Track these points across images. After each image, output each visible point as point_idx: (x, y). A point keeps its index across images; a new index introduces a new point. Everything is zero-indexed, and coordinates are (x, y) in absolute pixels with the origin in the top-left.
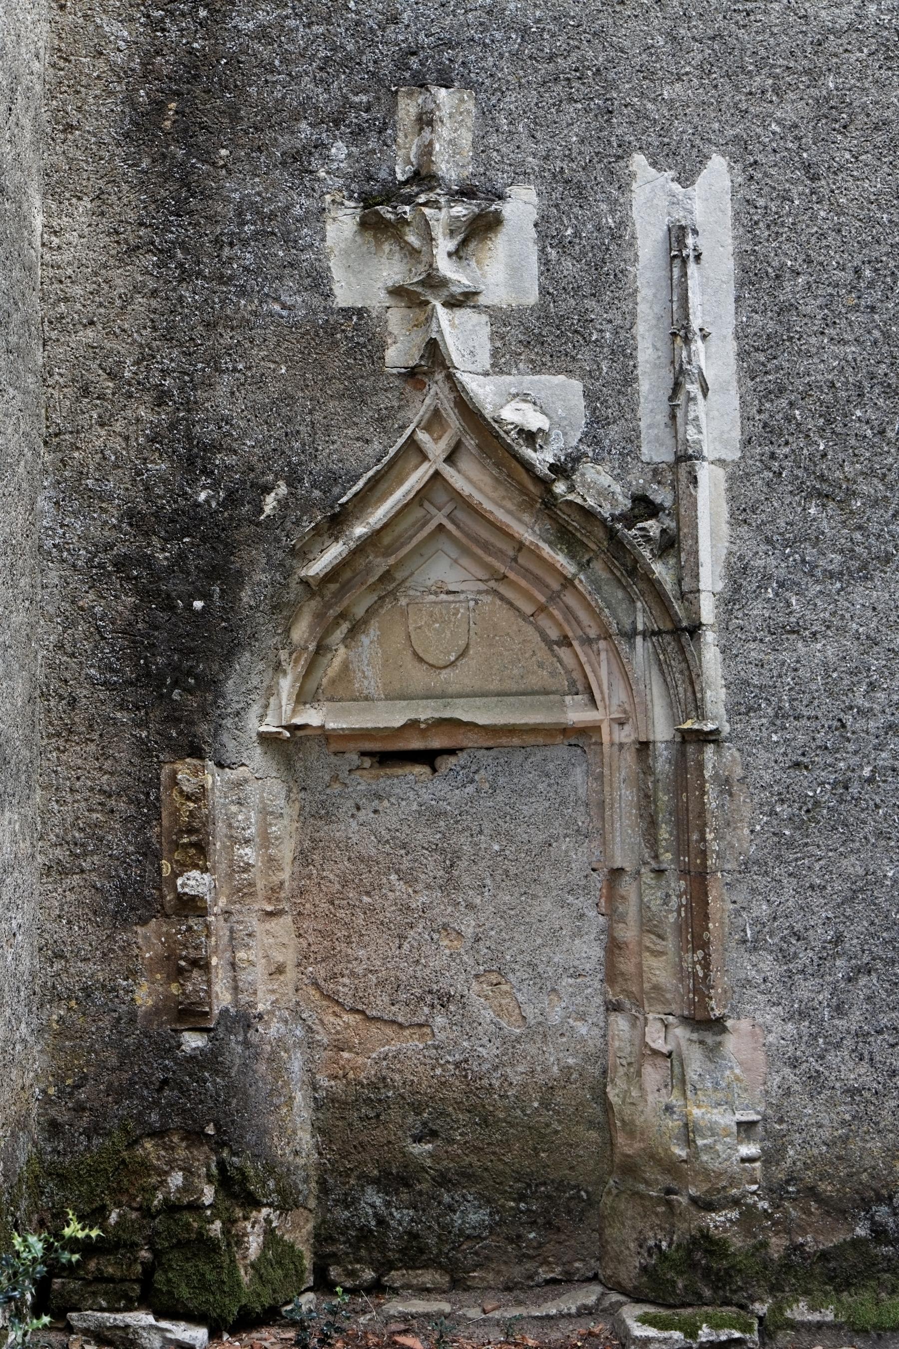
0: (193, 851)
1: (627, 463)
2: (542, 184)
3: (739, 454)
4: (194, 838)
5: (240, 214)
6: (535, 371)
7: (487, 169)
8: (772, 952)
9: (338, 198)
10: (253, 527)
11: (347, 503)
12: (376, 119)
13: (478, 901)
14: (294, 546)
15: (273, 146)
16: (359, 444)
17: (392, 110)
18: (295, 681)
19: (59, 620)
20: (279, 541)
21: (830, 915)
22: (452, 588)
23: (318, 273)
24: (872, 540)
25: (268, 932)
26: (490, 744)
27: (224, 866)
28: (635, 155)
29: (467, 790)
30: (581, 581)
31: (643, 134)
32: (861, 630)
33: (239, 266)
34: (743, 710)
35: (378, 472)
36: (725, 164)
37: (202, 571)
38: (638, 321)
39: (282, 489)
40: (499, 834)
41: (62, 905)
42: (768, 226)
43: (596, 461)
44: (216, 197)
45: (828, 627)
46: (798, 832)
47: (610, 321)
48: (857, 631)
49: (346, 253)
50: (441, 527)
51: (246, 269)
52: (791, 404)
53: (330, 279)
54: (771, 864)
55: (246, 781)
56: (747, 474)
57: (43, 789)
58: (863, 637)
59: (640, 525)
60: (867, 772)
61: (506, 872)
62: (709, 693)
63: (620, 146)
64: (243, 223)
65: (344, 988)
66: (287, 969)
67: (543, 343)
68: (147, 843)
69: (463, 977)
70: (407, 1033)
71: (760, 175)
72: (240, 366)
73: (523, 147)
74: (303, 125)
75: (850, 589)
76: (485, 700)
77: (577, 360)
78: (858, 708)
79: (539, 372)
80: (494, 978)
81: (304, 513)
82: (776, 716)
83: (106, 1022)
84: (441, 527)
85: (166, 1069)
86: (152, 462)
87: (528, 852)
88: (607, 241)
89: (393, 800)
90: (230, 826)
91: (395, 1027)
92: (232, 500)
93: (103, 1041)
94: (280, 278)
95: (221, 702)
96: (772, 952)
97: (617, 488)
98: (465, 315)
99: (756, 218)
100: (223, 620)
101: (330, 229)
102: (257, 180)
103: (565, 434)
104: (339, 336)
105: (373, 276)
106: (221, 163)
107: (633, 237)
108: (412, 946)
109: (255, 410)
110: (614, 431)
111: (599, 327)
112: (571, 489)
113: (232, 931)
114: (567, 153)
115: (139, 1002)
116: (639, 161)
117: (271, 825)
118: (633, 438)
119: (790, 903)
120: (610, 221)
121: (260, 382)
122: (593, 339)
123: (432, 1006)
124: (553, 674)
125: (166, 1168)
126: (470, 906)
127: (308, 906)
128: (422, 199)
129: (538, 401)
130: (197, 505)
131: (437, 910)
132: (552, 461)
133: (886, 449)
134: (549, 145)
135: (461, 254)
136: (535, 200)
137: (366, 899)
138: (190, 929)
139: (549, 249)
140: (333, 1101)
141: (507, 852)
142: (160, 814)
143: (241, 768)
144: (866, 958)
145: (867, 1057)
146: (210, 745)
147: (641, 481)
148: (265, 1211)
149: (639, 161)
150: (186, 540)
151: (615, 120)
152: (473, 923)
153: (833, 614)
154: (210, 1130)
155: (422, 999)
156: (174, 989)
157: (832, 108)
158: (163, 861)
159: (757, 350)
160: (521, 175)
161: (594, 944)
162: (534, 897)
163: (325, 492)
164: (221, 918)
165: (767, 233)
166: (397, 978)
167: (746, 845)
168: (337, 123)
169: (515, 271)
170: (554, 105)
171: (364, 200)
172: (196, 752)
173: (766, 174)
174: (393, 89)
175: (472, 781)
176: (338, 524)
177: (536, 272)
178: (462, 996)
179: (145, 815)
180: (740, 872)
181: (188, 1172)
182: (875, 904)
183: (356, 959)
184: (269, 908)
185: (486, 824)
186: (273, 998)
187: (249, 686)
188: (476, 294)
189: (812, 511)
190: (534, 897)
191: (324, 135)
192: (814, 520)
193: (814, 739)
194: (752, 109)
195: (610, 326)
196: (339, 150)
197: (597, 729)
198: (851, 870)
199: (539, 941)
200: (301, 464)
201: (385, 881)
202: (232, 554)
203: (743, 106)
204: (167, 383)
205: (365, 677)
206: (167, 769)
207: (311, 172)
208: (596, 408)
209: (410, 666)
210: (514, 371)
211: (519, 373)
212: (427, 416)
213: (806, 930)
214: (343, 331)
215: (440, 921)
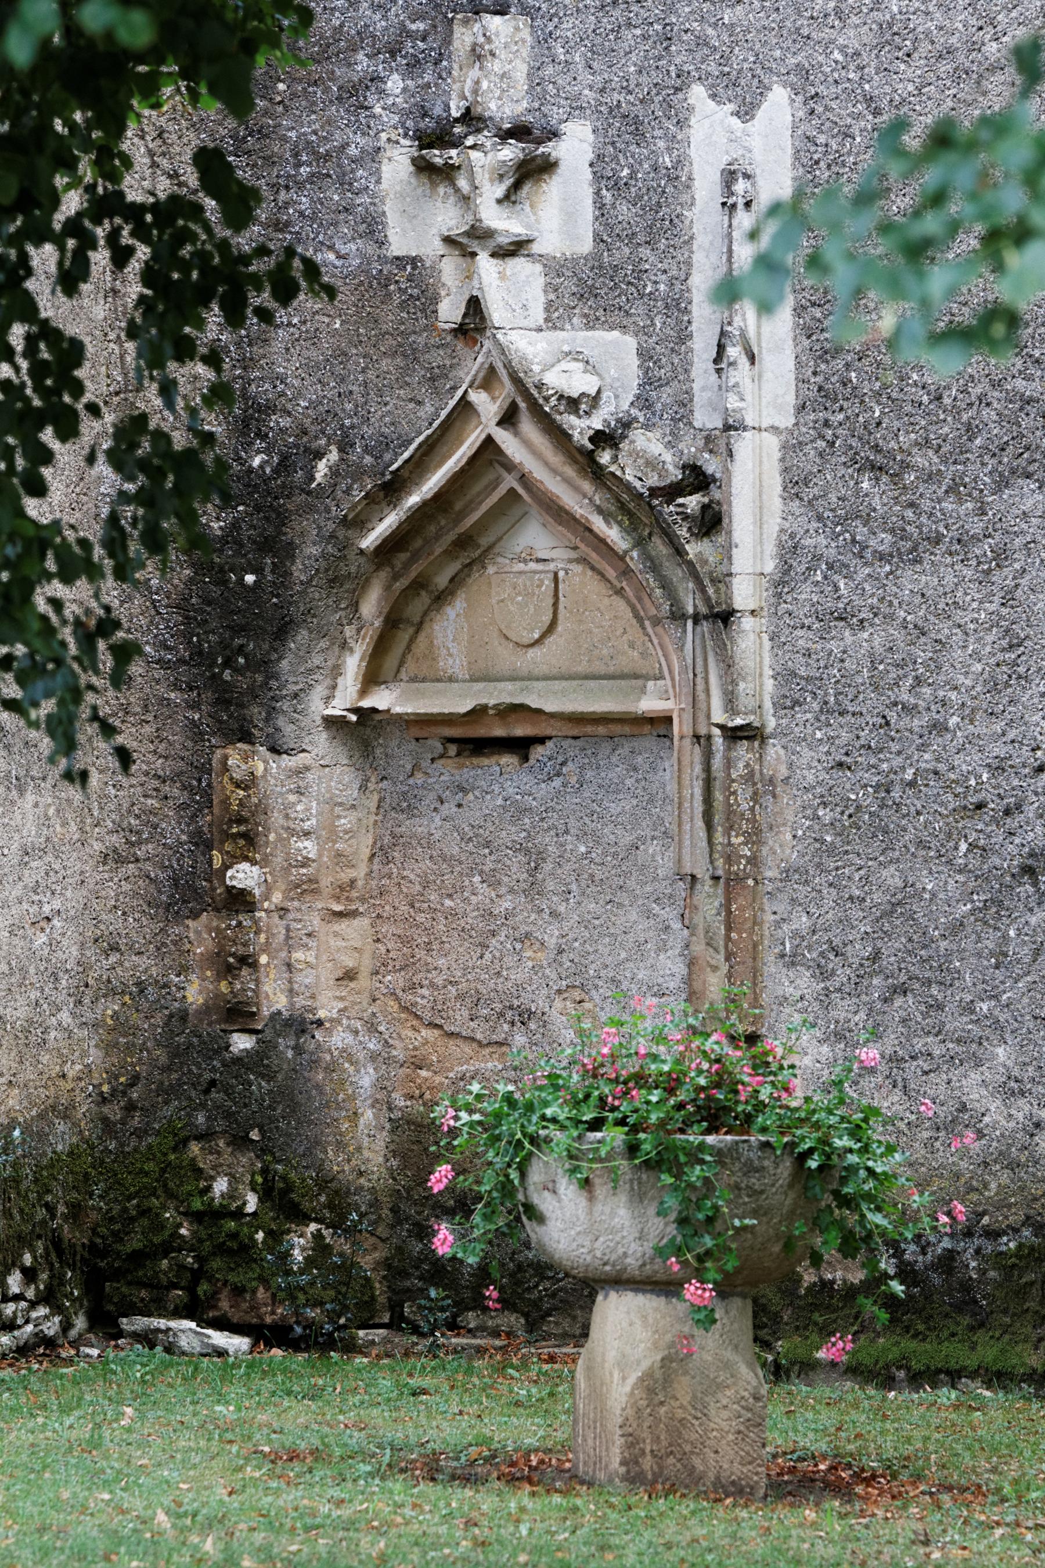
0: (242, 842)
1: (679, 429)
2: (598, 119)
3: (793, 421)
4: (243, 828)
5: (296, 155)
6: (589, 327)
7: (542, 104)
8: (809, 967)
9: (394, 138)
10: (304, 496)
11: (398, 469)
12: (432, 49)
13: (562, 909)
14: (345, 516)
15: (330, 80)
16: (412, 405)
17: (448, 41)
18: (361, 660)
19: (115, 593)
20: (329, 511)
21: (869, 930)
22: (541, 555)
23: (373, 218)
24: (924, 519)
25: (336, 934)
26: (575, 732)
27: (279, 859)
28: (693, 86)
29: (554, 784)
30: (632, 559)
31: (702, 63)
32: (909, 618)
33: (295, 210)
34: (789, 704)
35: (429, 437)
36: (786, 96)
37: (254, 542)
38: (694, 271)
39: (334, 456)
40: (586, 834)
41: (117, 895)
42: (829, 166)
43: (647, 427)
44: (273, 136)
45: (876, 615)
46: (839, 839)
47: (665, 272)
48: (905, 619)
49: (401, 196)
50: (512, 491)
51: (301, 214)
52: (848, 366)
53: (384, 225)
54: (811, 872)
55: (307, 768)
56: (800, 443)
57: (101, 772)
58: (911, 626)
59: (681, 500)
60: (909, 775)
61: (592, 876)
62: (742, 686)
63: (678, 76)
64: (298, 165)
65: (422, 998)
66: (359, 976)
67: (596, 296)
68: (199, 832)
69: (545, 992)
70: (488, 1050)
71: (821, 109)
72: (295, 321)
73: (579, 78)
74: (360, 56)
75: (899, 572)
76: (564, 683)
77: (631, 315)
78: (903, 704)
79: (592, 328)
80: (577, 994)
81: (354, 481)
82: (821, 711)
83: (159, 1019)
84: (512, 491)
85: (214, 1070)
86: (209, 423)
87: (615, 855)
88: (663, 183)
89: (477, 793)
90: (287, 817)
91: (475, 1045)
92: (285, 465)
93: (156, 1040)
94: (335, 224)
95: (274, 684)
96: (809, 967)
97: (668, 457)
98: (518, 265)
99: (816, 157)
100: (274, 596)
101: (386, 169)
102: (313, 117)
103: (616, 397)
104: (392, 287)
105: (428, 221)
106: (279, 99)
107: (690, 179)
108: (494, 957)
109: (311, 367)
110: (666, 395)
111: (653, 278)
112: (615, 459)
113: (288, 929)
114: (625, 84)
115: (190, 1000)
116: (698, 93)
117: (339, 817)
118: (685, 402)
119: (829, 916)
120: (667, 160)
121: (314, 338)
122: (648, 290)
123: (513, 1023)
124: (644, 655)
125: (212, 1173)
126: (553, 914)
127: (387, 908)
128: (470, 141)
129: (591, 360)
130: (250, 470)
131: (520, 917)
132: (600, 427)
133: (942, 417)
134: (606, 76)
135: (513, 198)
136: (591, 137)
137: (448, 903)
138: (239, 924)
139: (604, 192)
140: (408, 1123)
141: (594, 855)
142: (211, 801)
143: (302, 755)
144: (903, 978)
145: (900, 1084)
146: (261, 729)
147: (693, 449)
148: (313, 1227)
149: (698, 93)
150: (241, 508)
151: (673, 48)
152: (557, 933)
153: (882, 600)
154: (255, 1135)
155: (501, 1015)
156: (224, 987)
157: (895, 34)
158: (214, 852)
159: (814, 304)
160: (577, 109)
161: (679, 959)
162: (620, 905)
163: (376, 458)
164: (275, 915)
165: (827, 174)
166: (477, 992)
167: (788, 851)
168: (393, 54)
169: (569, 216)
170: (612, 30)
171: (419, 139)
172: (246, 737)
173: (827, 108)
174: (450, 15)
175: (558, 775)
176: (395, 491)
177: (590, 217)
178: (543, 1014)
179: (197, 802)
180: (781, 880)
181: (233, 1179)
182: (914, 920)
183: (436, 969)
184: (338, 908)
185: (572, 822)
186: (341, 1005)
187: (309, 665)
188: (529, 241)
189: (865, 485)
190: (620, 905)
191: (381, 67)
192: (867, 495)
193: (858, 738)
194: (814, 35)
195: (664, 277)
196: (395, 84)
197: (669, 720)
198: (890, 881)
199: (623, 955)
200: (353, 427)
201: (467, 883)
202: (284, 524)
203: (805, 31)
204: (223, 338)
205: (450, 655)
206: (219, 753)
207: (367, 108)
208: (649, 368)
209: (496, 643)
210: (568, 326)
211: (573, 329)
212: (481, 375)
213: (845, 945)
214: (397, 282)
215: (524, 929)
